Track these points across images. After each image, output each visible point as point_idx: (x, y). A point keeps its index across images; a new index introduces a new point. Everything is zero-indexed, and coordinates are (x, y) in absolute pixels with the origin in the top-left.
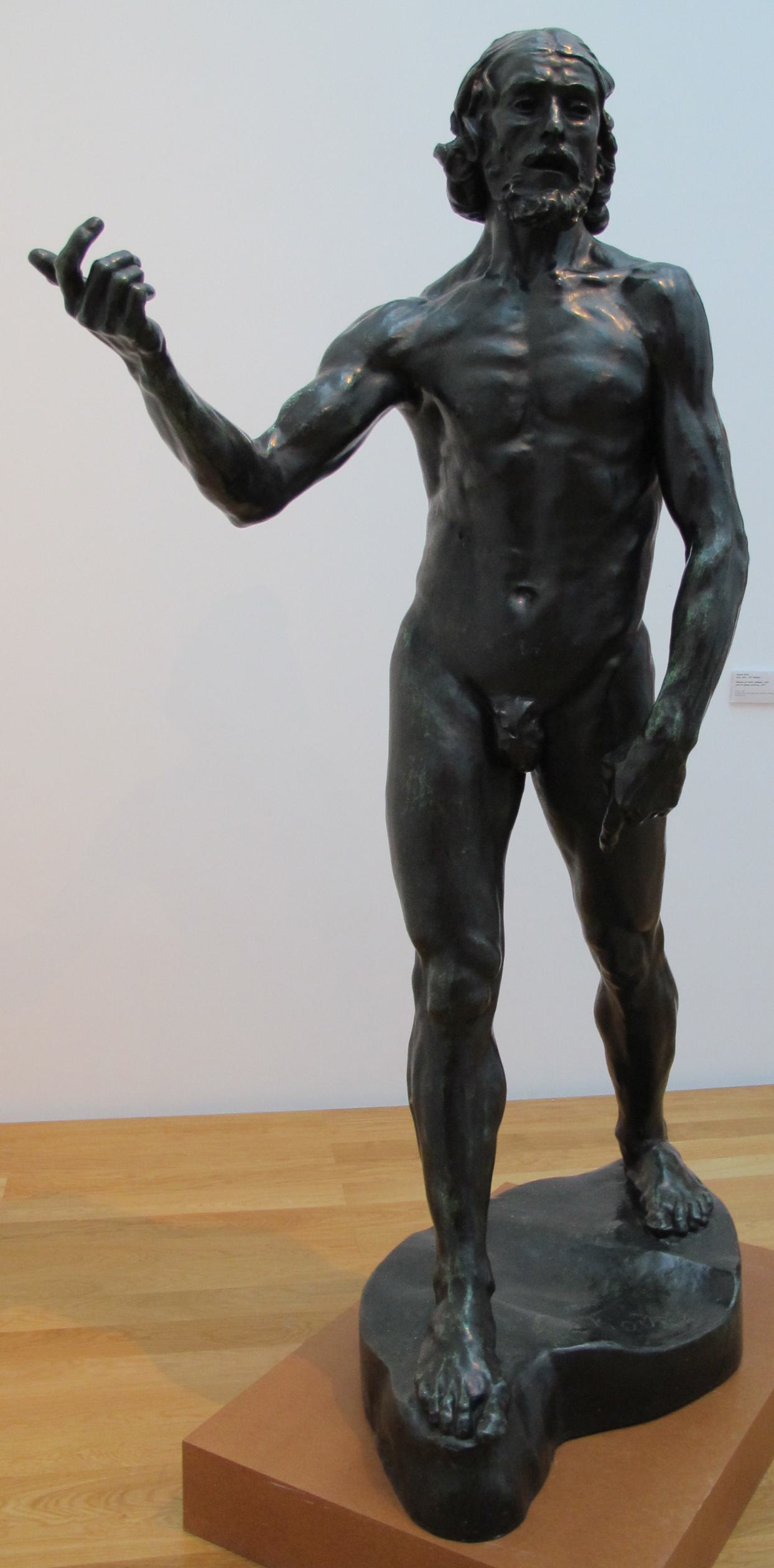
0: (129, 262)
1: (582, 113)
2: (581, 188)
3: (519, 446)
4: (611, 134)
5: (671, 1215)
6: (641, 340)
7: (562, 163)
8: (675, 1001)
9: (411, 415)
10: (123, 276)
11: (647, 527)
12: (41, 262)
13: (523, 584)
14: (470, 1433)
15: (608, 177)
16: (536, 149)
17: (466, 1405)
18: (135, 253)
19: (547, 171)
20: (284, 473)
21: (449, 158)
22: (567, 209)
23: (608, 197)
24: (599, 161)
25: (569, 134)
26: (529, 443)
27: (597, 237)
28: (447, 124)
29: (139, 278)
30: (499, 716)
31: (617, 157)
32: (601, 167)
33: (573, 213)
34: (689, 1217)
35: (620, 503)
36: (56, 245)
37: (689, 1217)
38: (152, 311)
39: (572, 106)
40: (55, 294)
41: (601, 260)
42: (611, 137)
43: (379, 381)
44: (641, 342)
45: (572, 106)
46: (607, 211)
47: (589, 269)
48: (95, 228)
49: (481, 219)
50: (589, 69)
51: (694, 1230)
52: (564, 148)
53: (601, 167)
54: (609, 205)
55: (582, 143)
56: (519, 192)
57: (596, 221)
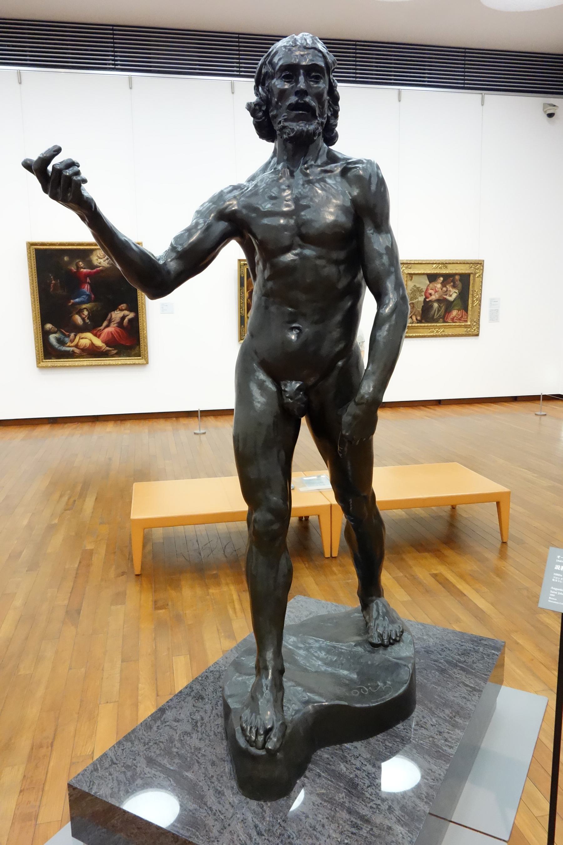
0: (72, 164)
1: (317, 79)
2: (318, 120)
3: (290, 257)
4: (336, 90)
5: (380, 636)
6: (350, 199)
7: (307, 107)
8: (383, 531)
9: (242, 244)
10: (68, 172)
11: (357, 296)
12: (28, 166)
13: (294, 325)
14: (263, 747)
15: (335, 114)
16: (293, 99)
17: (262, 733)
18: (75, 159)
19: (298, 112)
20: (172, 272)
21: (253, 109)
22: (310, 132)
23: (336, 125)
24: (330, 105)
25: (309, 91)
26: (295, 255)
27: (330, 147)
28: (254, 95)
29: (78, 173)
30: (285, 391)
31: (340, 103)
32: (332, 109)
33: (314, 134)
34: (390, 638)
35: (342, 284)
36: (34, 157)
37: (390, 638)
38: (88, 190)
39: (312, 75)
40: (33, 181)
41: (333, 158)
42: (336, 92)
43: (222, 226)
44: (350, 201)
45: (312, 75)
46: (337, 133)
47: (326, 164)
48: (58, 151)
49: (273, 141)
50: (321, 55)
51: (392, 644)
52: (308, 99)
53: (332, 109)
54: (337, 129)
55: (319, 97)
56: (286, 124)
57: (331, 138)
